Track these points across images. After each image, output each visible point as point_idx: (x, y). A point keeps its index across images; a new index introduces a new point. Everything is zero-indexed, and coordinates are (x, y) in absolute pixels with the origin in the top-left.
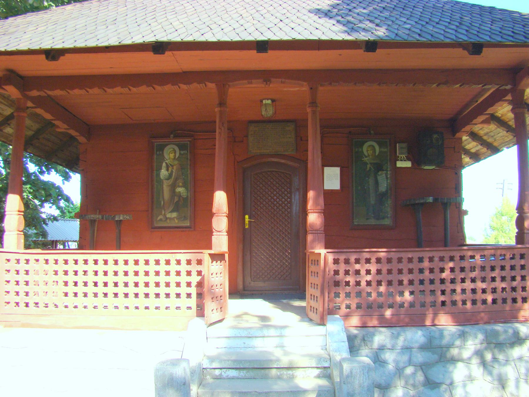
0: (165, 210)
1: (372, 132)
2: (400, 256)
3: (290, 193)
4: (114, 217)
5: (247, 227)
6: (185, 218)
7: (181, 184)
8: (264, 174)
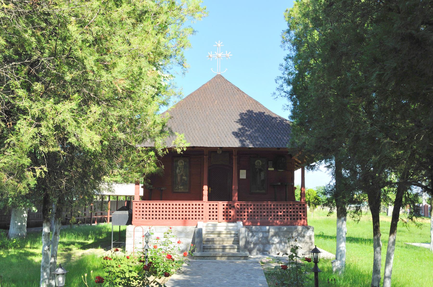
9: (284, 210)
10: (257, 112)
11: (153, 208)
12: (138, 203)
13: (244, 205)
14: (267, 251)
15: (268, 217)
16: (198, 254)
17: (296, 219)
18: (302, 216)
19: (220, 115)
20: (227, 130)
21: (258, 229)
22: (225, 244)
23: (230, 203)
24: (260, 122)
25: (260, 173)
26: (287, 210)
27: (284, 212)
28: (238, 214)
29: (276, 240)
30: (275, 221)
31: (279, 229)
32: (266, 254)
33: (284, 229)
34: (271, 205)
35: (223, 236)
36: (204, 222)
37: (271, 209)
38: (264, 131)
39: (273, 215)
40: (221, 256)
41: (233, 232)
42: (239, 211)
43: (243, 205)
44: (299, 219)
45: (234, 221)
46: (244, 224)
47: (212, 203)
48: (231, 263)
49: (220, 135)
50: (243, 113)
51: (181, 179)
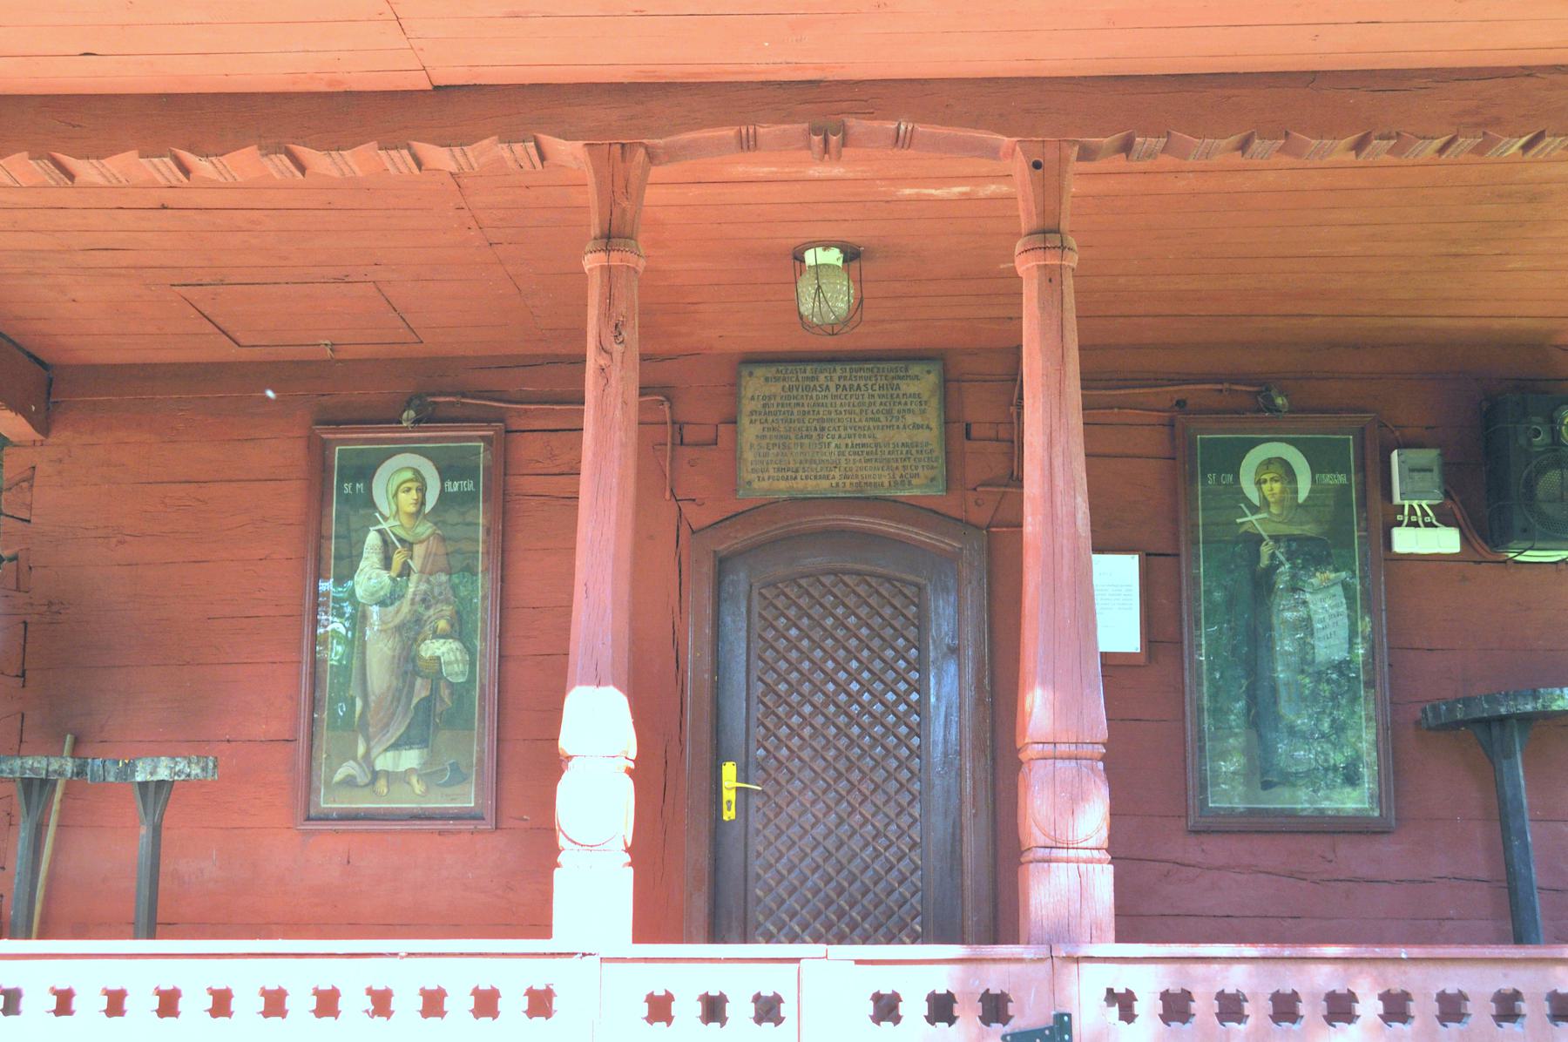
0: (368, 740)
1: (1279, 401)
2: (1507, 986)
3: (921, 665)
4: (131, 768)
5: (729, 814)
6: (458, 775)
7: (442, 624)
8: (803, 582)
47: (693, 970)
51: (408, 665)
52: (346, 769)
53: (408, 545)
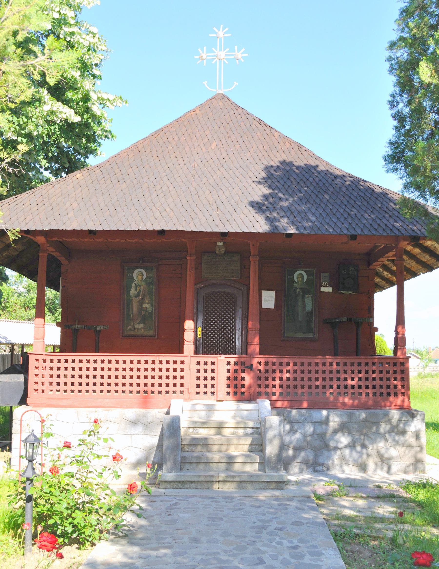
6: (150, 329)
7: (147, 301)
9: (360, 375)
10: (302, 165)
11: (124, 370)
12: (41, 358)
13: (274, 364)
14: (323, 465)
15: (324, 390)
16: (171, 476)
17: (385, 394)
18: (399, 387)
19: (222, 170)
20: (237, 198)
21: (302, 415)
22: (233, 452)
23: (243, 360)
24: (308, 184)
25: (303, 297)
26: (367, 376)
27: (360, 379)
28: (259, 382)
29: (344, 440)
30: (341, 399)
31: (350, 416)
32: (320, 472)
33: (359, 415)
34: (331, 364)
35: (226, 432)
36: (185, 400)
37: (331, 372)
38: (318, 201)
39: (335, 386)
40: (224, 481)
41: (251, 424)
42: (263, 375)
43: (270, 364)
44: (392, 394)
45: (252, 398)
46: (273, 405)
47: (202, 358)
48: (247, 501)
49: (222, 207)
50: (272, 166)
52: (130, 327)
53: (140, 286)
